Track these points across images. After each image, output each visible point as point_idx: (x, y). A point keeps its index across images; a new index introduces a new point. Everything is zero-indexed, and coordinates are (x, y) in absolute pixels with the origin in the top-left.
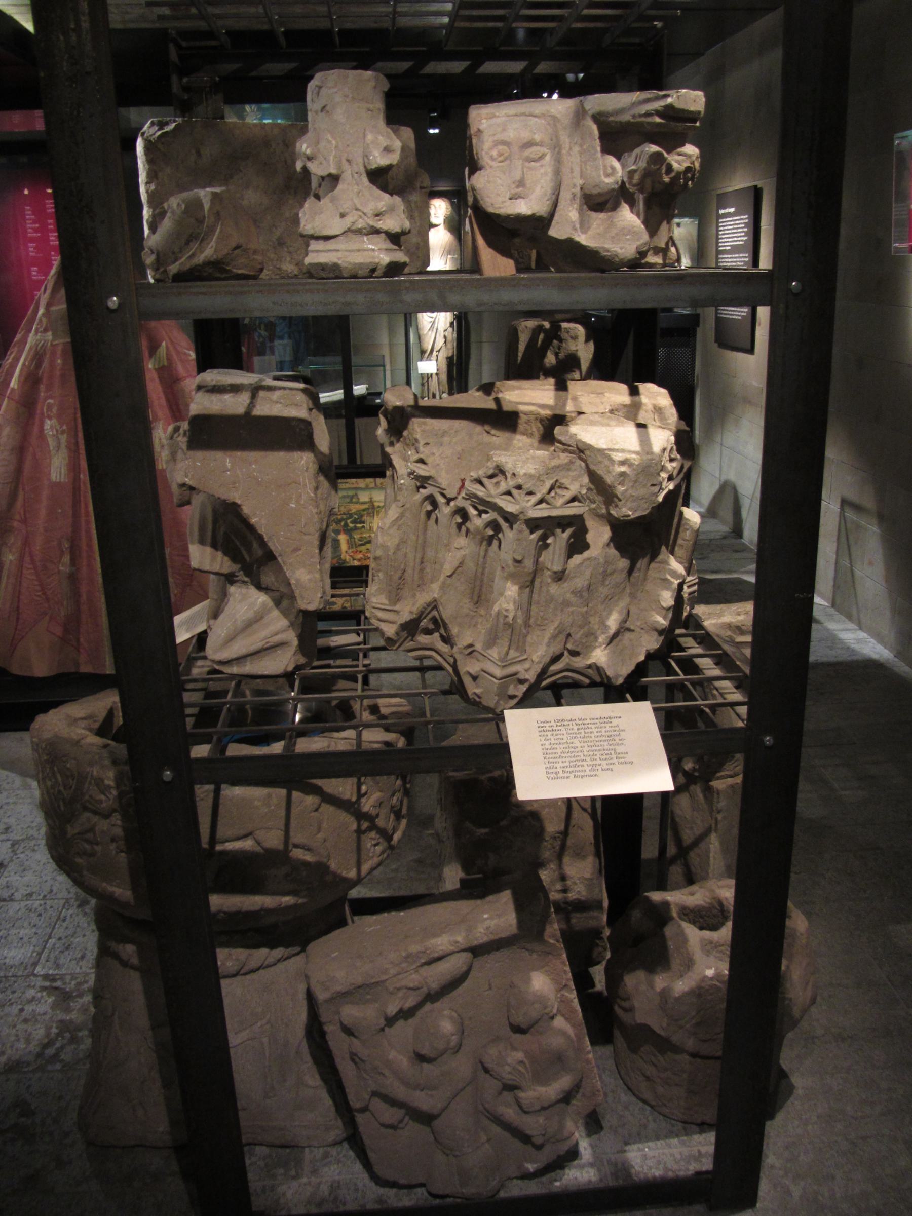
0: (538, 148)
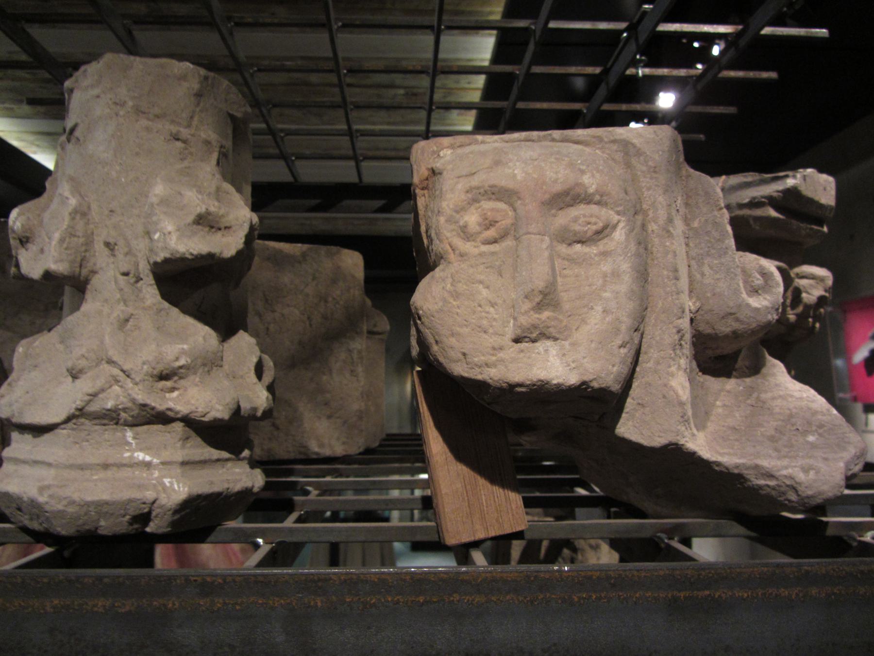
0: (594, 208)
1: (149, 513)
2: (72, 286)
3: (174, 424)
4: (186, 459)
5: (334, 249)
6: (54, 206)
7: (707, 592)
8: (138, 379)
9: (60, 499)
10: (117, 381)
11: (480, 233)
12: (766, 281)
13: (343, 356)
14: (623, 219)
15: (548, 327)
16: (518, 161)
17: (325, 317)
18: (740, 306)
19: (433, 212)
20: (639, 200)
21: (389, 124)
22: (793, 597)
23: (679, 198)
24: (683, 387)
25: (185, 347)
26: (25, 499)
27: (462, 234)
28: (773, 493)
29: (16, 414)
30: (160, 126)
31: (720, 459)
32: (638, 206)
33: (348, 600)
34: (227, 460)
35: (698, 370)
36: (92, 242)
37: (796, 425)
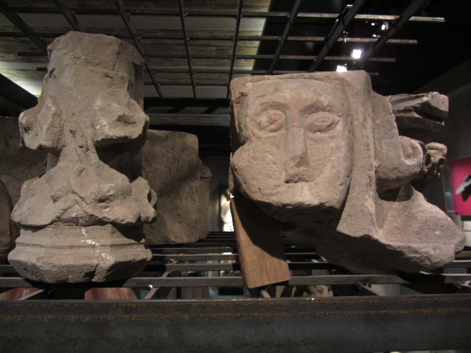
0: (326, 114)
1: (94, 271)
2: (53, 153)
3: (107, 225)
4: (113, 243)
5: (183, 133)
6: (43, 111)
7: (385, 311)
8: (88, 202)
9: (48, 264)
10: (77, 203)
11: (267, 126)
12: (414, 151)
13: (187, 190)
14: (342, 119)
15: (303, 175)
16: (287, 89)
17: (178, 170)
19: (242, 115)
20: (349, 110)
21: (208, 65)
22: (429, 314)
23: (370, 108)
24: (372, 206)
25: (113, 185)
26: (30, 264)
27: (258, 127)
28: (418, 261)
29: (24, 220)
31: (390, 243)
32: (349, 112)
33: (201, 315)
34: (134, 244)
35: (378, 197)
36: (63, 130)
37: (429, 226)
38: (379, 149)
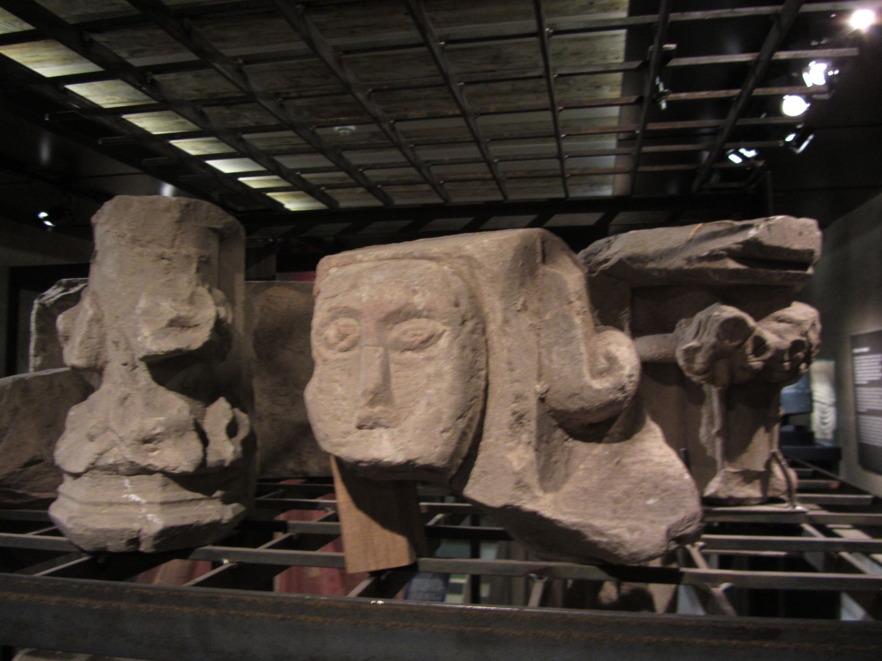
0: (422, 322)
4: (164, 500)
7: (488, 629)
18: (582, 388)
30: (149, 250)
34: (201, 499)
38: (546, 362)
